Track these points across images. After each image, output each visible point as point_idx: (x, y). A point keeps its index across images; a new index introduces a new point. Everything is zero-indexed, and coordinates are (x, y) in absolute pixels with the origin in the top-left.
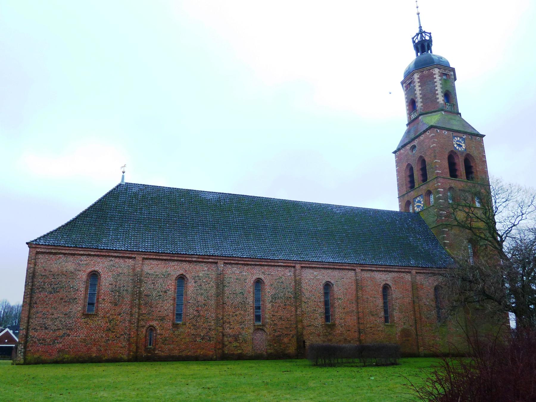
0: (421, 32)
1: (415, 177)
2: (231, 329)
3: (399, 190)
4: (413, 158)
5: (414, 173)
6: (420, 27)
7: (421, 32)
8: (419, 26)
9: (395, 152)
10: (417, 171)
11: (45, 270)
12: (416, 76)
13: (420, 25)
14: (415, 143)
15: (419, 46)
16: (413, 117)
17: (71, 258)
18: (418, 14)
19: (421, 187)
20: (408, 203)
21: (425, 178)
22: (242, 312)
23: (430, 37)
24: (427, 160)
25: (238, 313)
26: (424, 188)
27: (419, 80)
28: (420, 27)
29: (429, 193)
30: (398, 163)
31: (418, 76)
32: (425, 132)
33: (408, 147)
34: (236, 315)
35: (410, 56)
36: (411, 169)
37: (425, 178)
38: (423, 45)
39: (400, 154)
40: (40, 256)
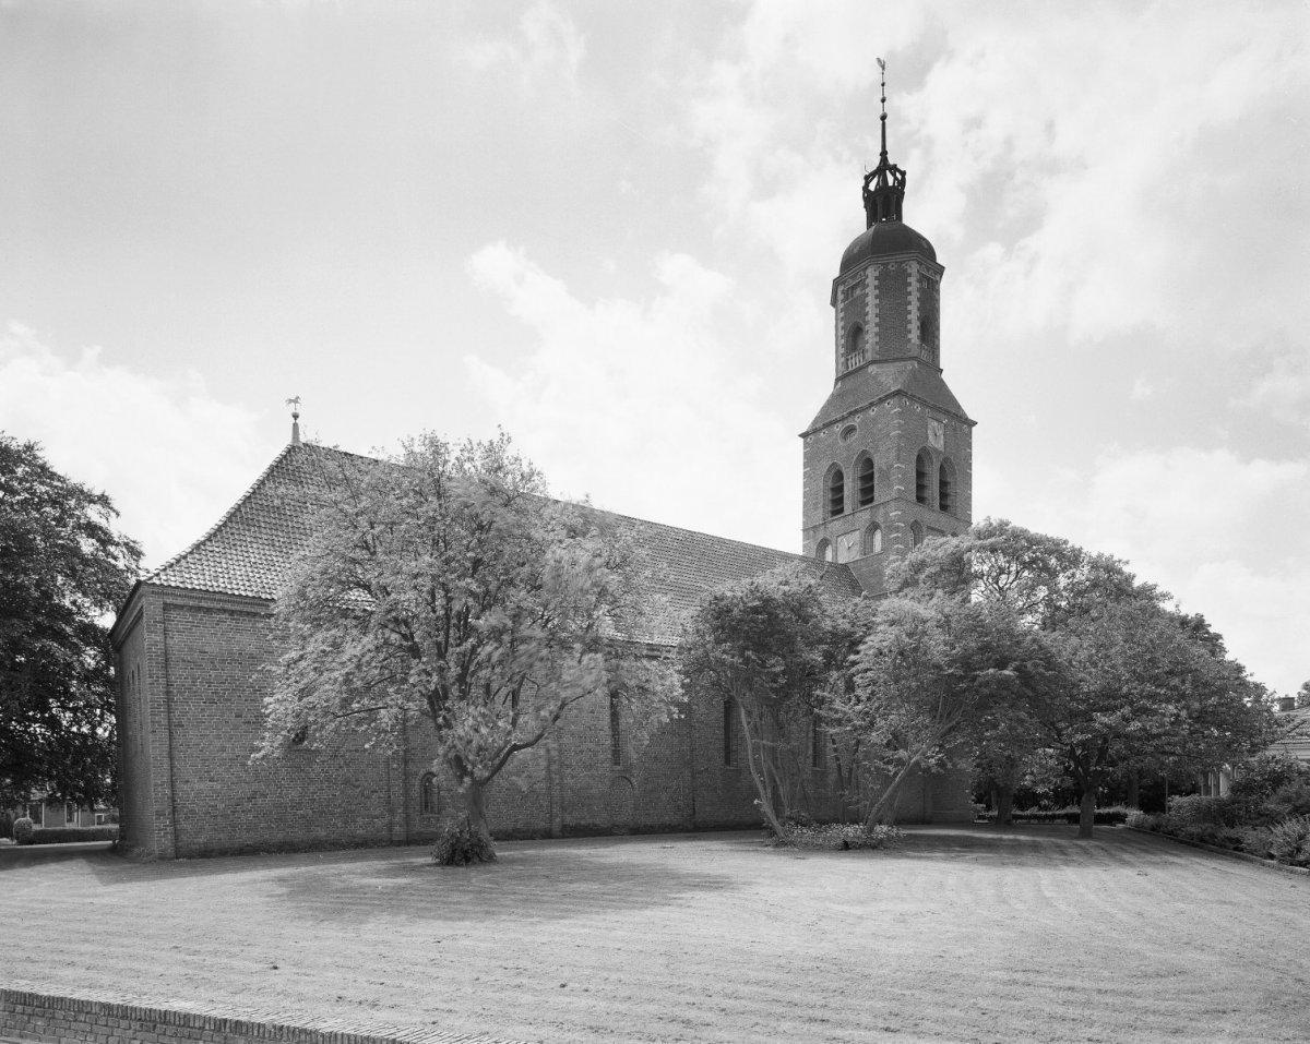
0: (885, 166)
1: (847, 492)
2: (573, 777)
3: (805, 514)
4: (845, 457)
5: (841, 487)
6: (884, 153)
7: (885, 166)
8: (880, 150)
9: (802, 436)
10: (854, 480)
11: (191, 649)
12: (872, 274)
13: (884, 146)
14: (856, 421)
15: (879, 201)
16: (856, 362)
17: (247, 624)
18: (883, 118)
19: (858, 514)
20: (824, 544)
21: (867, 495)
22: (592, 746)
23: (902, 183)
24: (879, 462)
25: (584, 747)
26: (864, 516)
27: (877, 283)
28: (884, 153)
29: (874, 527)
30: (810, 459)
31: (877, 274)
32: (881, 401)
33: (839, 428)
34: (582, 752)
35: (855, 222)
36: (839, 476)
37: (867, 495)
38: (884, 197)
39: (816, 442)
40: (173, 614)
